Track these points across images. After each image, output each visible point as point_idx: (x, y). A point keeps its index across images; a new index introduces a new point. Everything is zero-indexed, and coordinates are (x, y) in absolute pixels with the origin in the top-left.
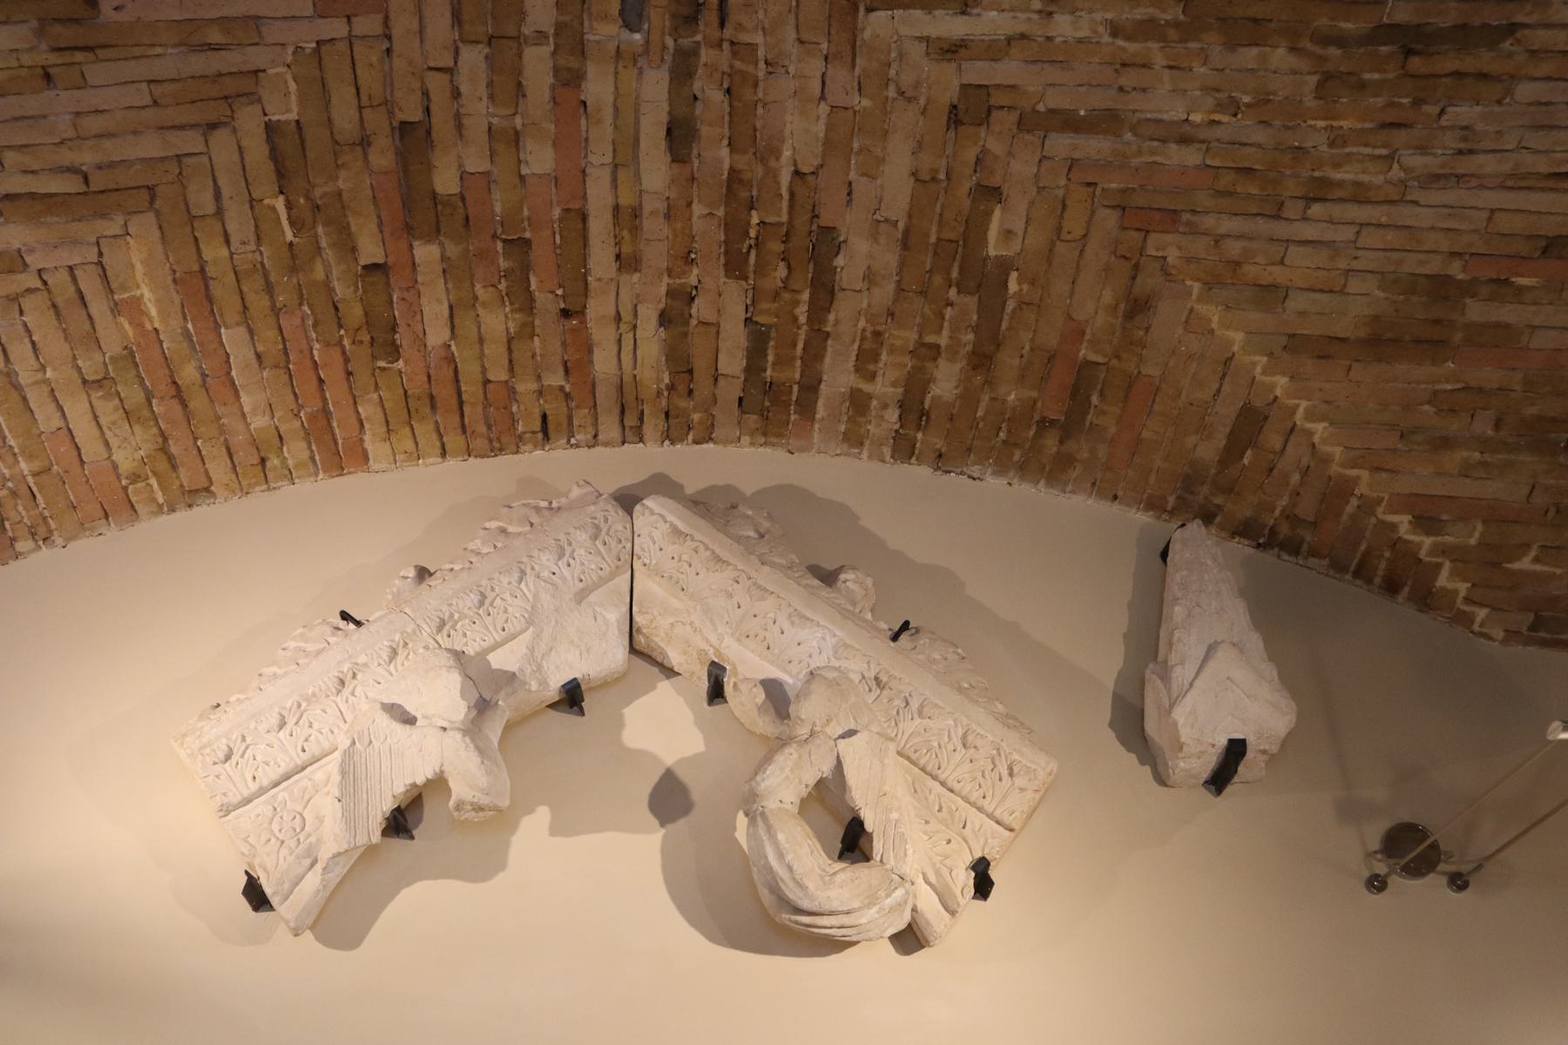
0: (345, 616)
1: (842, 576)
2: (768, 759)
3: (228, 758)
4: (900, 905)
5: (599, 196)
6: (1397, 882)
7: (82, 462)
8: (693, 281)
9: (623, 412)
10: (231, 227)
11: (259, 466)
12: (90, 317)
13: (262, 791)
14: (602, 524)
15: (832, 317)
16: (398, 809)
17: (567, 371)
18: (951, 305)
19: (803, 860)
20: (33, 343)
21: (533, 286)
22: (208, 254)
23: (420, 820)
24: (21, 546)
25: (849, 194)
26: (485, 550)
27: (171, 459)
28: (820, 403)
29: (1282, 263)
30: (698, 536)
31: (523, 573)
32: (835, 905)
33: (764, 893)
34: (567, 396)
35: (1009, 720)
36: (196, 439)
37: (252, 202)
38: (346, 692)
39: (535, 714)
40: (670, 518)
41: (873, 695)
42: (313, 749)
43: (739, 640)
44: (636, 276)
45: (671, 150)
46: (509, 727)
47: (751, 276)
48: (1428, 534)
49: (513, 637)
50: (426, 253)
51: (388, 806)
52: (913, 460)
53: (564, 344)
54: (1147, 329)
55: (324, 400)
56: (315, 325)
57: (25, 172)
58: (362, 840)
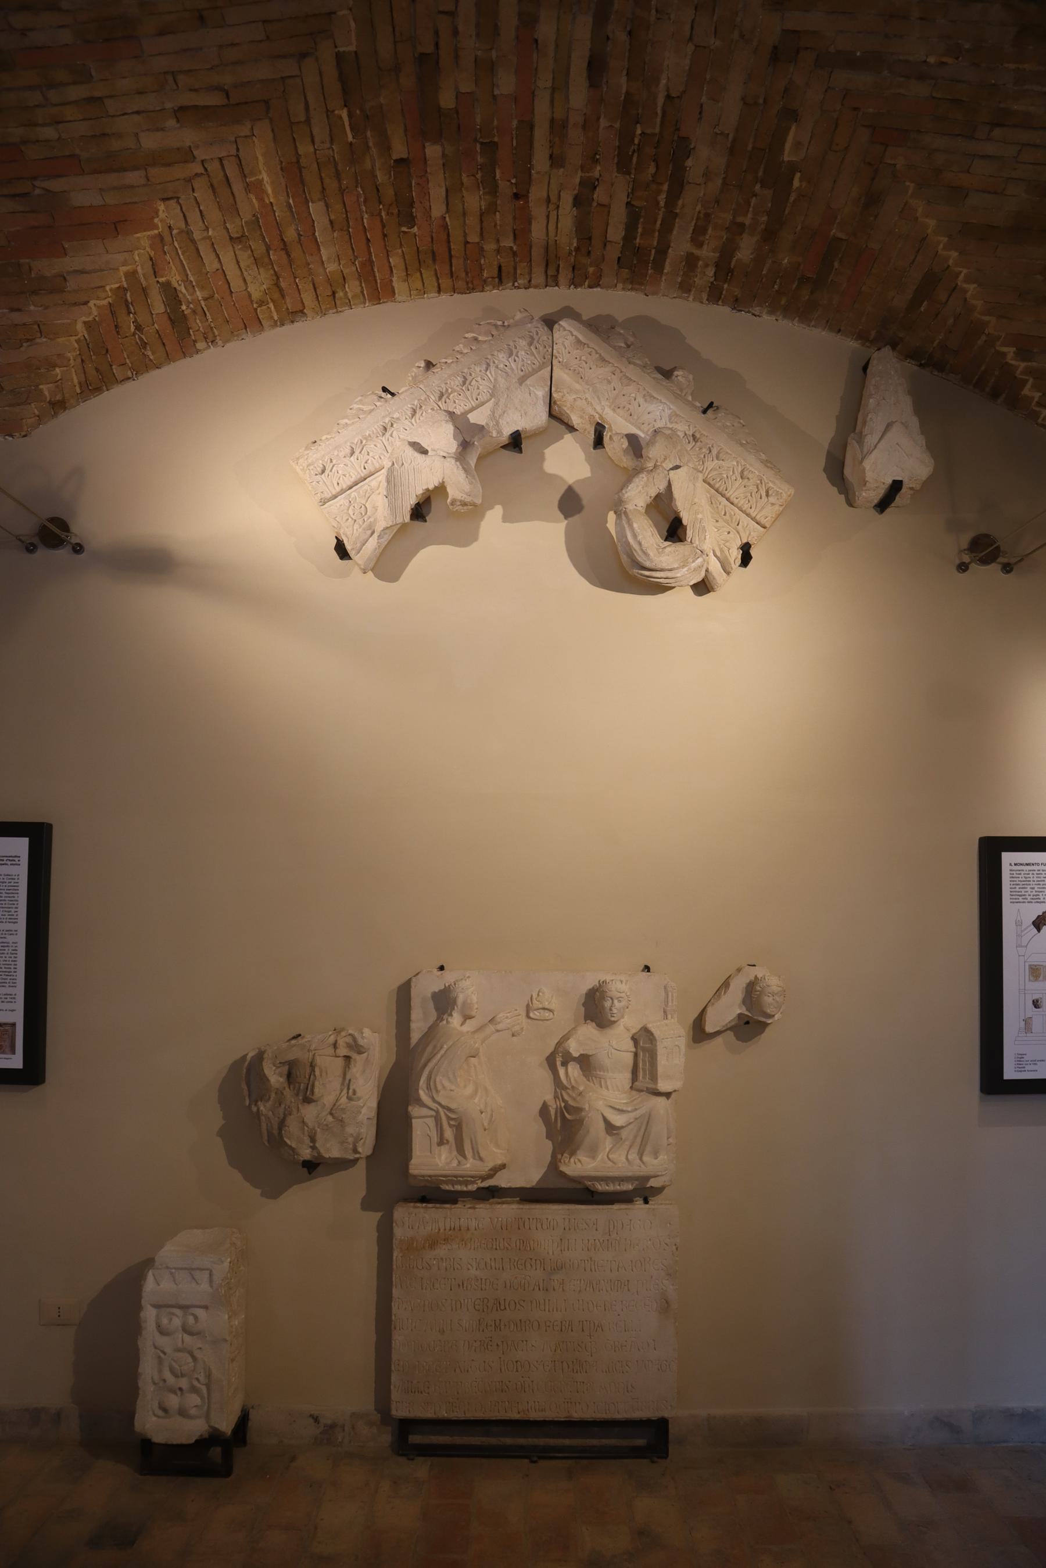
0: (385, 390)
1: (676, 373)
2: (629, 480)
3: (323, 472)
4: (700, 567)
5: (542, 109)
6: (974, 567)
7: (231, 292)
8: (597, 174)
9: (547, 265)
10: (315, 132)
11: (331, 298)
12: (232, 193)
13: (343, 491)
14: (535, 336)
15: (680, 202)
16: (418, 504)
17: (515, 238)
18: (756, 195)
19: (646, 537)
20: (201, 211)
21: (498, 177)
22: (301, 150)
23: (429, 512)
24: (200, 345)
25: (700, 113)
26: (465, 351)
27: (281, 291)
28: (668, 261)
29: (968, 172)
30: (592, 345)
31: (488, 365)
32: (664, 566)
33: (624, 559)
34: (515, 254)
35: (768, 463)
36: (295, 278)
37: (329, 113)
38: (388, 434)
39: (494, 451)
40: (575, 333)
41: (691, 446)
42: (370, 468)
43: (614, 410)
44: (562, 170)
45: (590, 78)
46: (480, 458)
47: (633, 171)
48: (1024, 360)
49: (482, 404)
50: (433, 151)
51: (413, 501)
52: (720, 303)
53: (514, 218)
54: (876, 216)
55: (370, 253)
56: (365, 202)
57: (191, 90)
58: (399, 520)
